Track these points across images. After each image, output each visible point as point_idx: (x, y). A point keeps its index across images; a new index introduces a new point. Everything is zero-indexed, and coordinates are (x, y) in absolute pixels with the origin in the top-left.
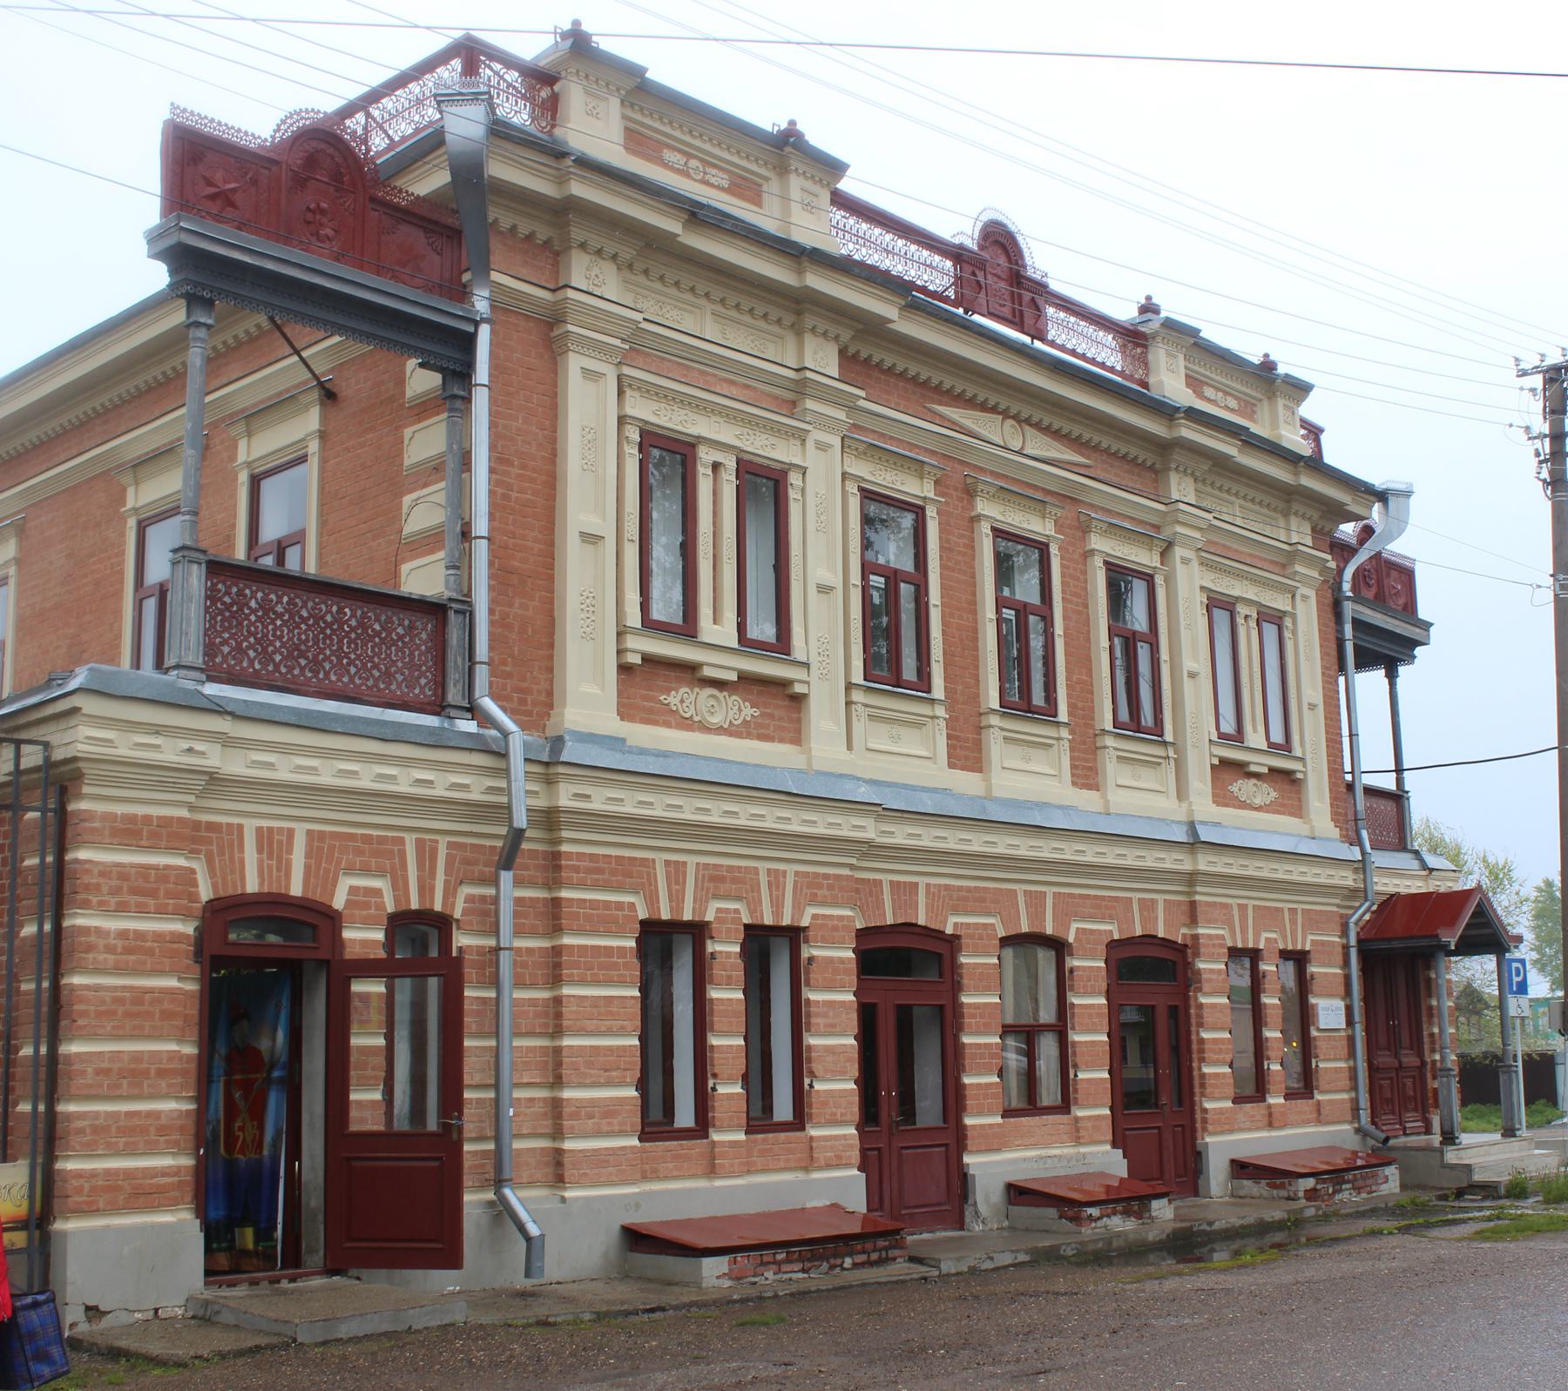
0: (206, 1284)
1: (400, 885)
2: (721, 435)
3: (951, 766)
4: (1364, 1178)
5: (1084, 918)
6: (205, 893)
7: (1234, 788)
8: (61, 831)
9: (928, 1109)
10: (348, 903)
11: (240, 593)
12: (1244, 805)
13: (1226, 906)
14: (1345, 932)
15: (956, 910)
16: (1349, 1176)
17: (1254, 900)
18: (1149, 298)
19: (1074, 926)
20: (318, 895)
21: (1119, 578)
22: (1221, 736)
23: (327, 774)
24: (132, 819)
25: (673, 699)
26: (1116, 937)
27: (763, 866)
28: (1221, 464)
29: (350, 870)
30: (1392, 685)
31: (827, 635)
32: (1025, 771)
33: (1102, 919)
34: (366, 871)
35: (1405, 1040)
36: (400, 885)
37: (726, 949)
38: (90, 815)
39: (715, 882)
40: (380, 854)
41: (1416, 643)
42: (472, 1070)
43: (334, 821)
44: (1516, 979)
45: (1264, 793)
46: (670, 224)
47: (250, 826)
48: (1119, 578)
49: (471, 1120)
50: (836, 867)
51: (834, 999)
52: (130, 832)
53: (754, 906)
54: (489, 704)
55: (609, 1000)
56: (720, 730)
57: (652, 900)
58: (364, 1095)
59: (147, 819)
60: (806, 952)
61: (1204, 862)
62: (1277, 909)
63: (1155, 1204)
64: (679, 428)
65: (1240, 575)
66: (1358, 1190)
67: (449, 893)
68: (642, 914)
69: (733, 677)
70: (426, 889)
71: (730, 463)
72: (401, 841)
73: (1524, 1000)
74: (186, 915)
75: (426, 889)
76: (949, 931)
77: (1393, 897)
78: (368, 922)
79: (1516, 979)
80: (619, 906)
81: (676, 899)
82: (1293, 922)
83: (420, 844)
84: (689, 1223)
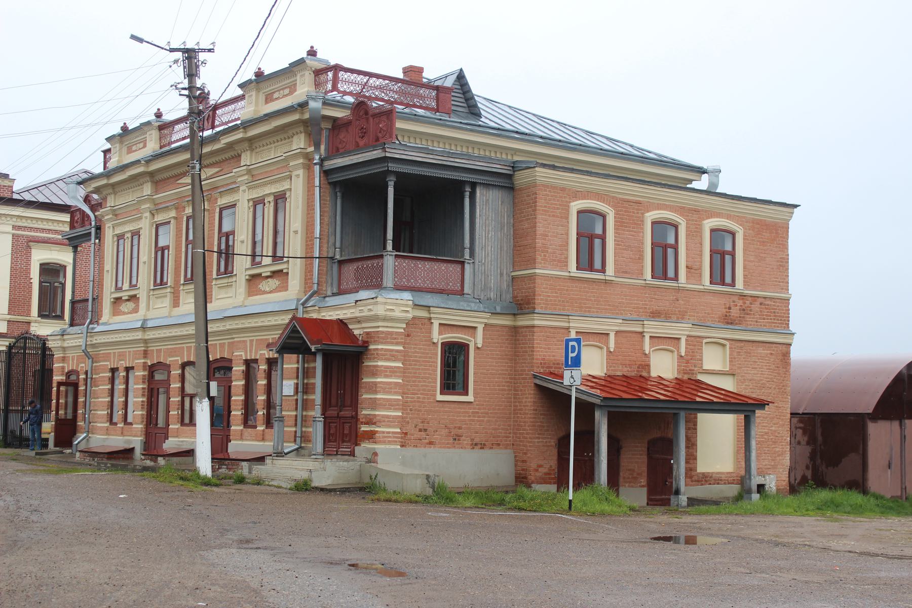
0: (648, 504)
4: (233, 465)
9: (161, 423)
12: (265, 292)
13: (244, 341)
16: (226, 462)
18: (312, 47)
28: (251, 140)
31: (145, 279)
35: (348, 402)
37: (238, 368)
39: (172, 352)
42: (80, 405)
44: (571, 355)
45: (274, 283)
49: (80, 417)
51: (137, 386)
56: (270, 292)
58: (61, 412)
61: (150, 335)
63: (159, 459)
65: (265, 184)
66: (230, 469)
69: (269, 274)
73: (576, 373)
74: (62, 375)
79: (571, 355)
82: (251, 345)
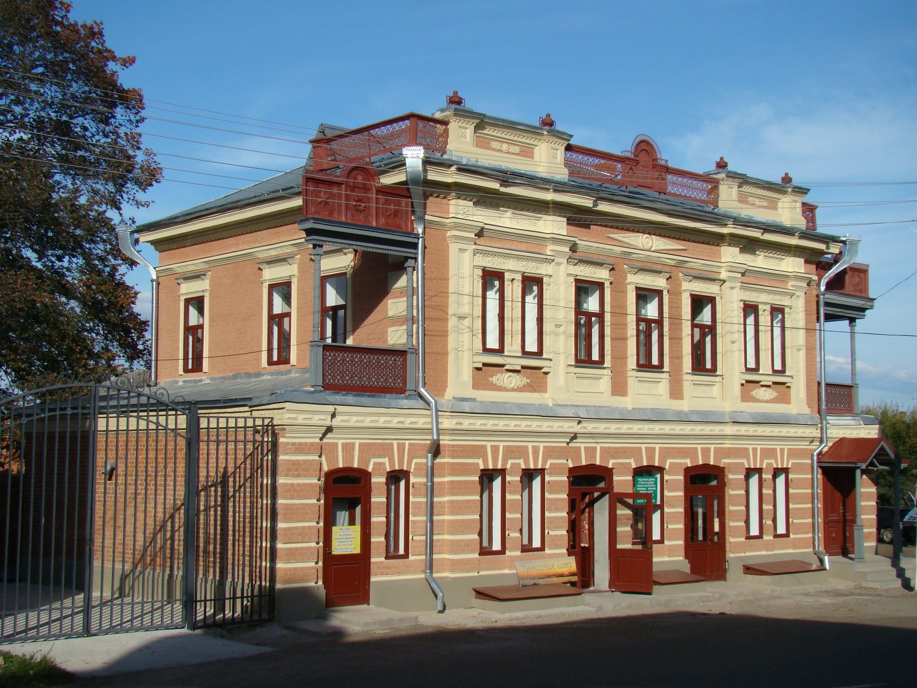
1: (391, 461)
2: (514, 268)
3: (671, 398)
5: (673, 458)
6: (326, 468)
7: (754, 393)
8: (274, 448)
10: (373, 469)
11: (395, 360)
14: (812, 460)
15: (614, 457)
17: (760, 446)
19: (373, 461)
20: (362, 467)
21: (698, 303)
22: (748, 369)
23: (368, 421)
24: (300, 444)
25: (494, 379)
26: (689, 465)
27: (750, 447)
29: (374, 456)
30: (852, 333)
31: (561, 344)
32: (648, 392)
33: (683, 457)
34: (380, 456)
36: (391, 461)
37: (513, 478)
38: (445, 445)
39: (510, 452)
40: (385, 450)
41: (863, 310)
43: (609, 444)
46: (495, 185)
47: (340, 442)
48: (698, 303)
50: (561, 442)
52: (300, 448)
53: (527, 461)
54: (422, 390)
55: (468, 501)
57: (485, 461)
59: (306, 443)
60: (791, 476)
62: (524, 447)
64: (532, 271)
67: (410, 462)
68: (482, 467)
70: (401, 461)
71: (519, 277)
72: (392, 444)
75: (401, 461)
76: (610, 466)
77: (842, 440)
78: (380, 475)
80: (473, 464)
81: (495, 460)
83: (398, 444)
84: (492, 588)
